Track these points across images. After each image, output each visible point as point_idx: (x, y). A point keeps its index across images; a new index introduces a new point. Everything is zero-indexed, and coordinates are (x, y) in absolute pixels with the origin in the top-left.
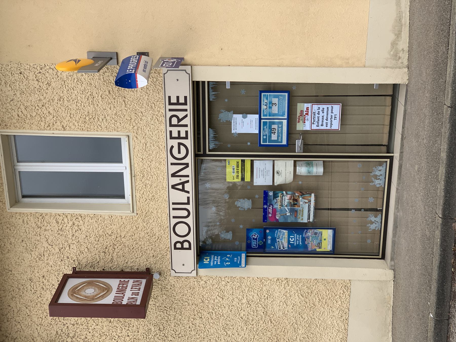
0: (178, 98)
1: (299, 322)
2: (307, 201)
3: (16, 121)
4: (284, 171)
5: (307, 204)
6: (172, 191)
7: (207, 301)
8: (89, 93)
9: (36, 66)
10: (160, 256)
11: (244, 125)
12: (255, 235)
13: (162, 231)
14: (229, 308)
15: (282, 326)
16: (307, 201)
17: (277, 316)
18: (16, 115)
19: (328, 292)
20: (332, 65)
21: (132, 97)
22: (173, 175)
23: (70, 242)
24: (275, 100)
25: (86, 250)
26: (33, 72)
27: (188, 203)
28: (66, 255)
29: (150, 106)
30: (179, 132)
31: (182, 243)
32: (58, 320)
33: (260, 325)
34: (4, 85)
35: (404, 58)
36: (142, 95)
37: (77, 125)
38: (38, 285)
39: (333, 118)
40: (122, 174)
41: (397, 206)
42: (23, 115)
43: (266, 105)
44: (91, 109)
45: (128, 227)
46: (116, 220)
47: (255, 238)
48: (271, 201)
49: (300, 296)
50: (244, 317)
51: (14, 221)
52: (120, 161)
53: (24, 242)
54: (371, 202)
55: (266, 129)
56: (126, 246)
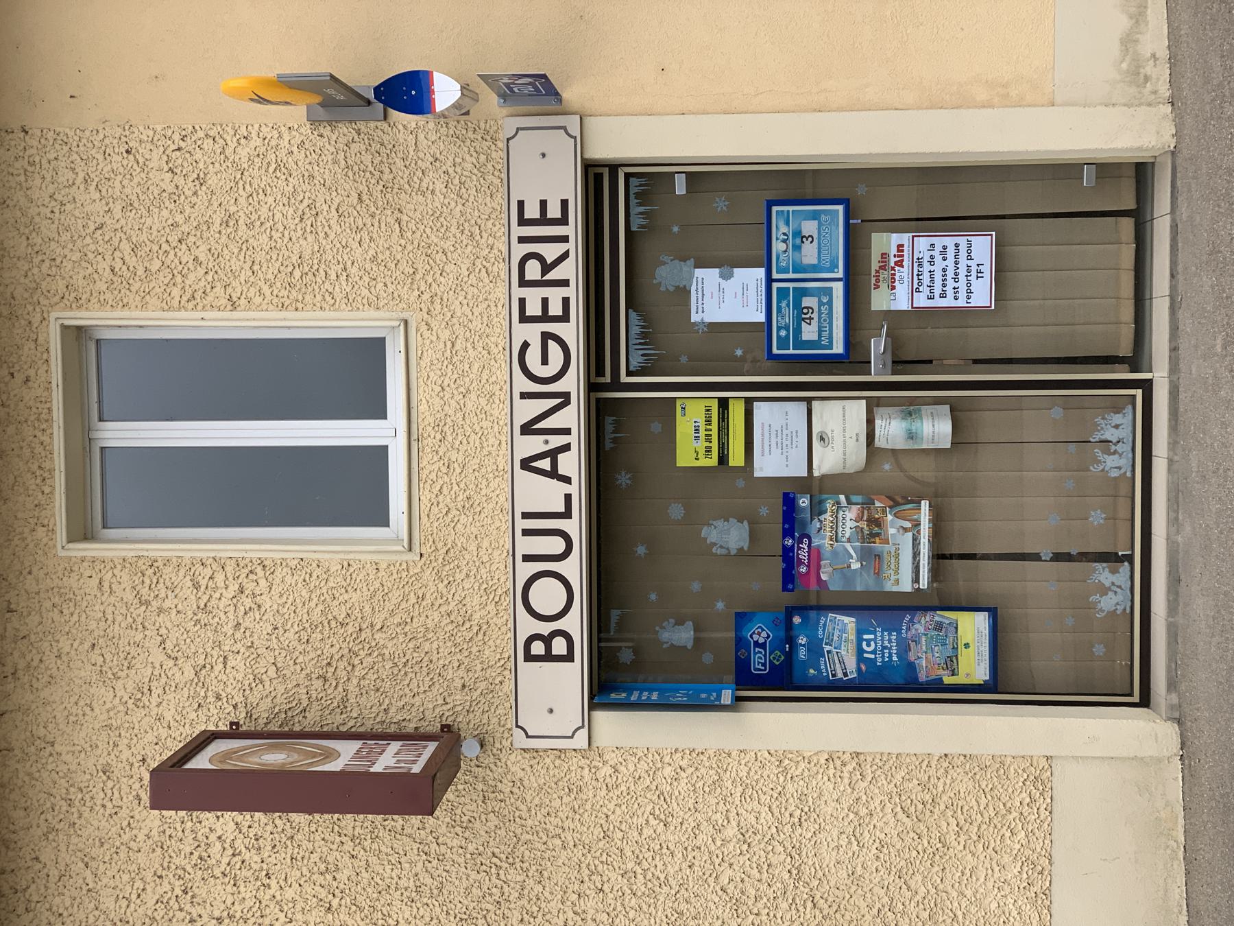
0: (543, 204)
1: (899, 905)
2: (908, 525)
3: (104, 287)
4: (839, 431)
5: (910, 534)
6: (522, 476)
7: (620, 835)
8: (306, 202)
9: (169, 133)
10: (483, 685)
11: (727, 297)
12: (759, 632)
13: (491, 607)
14: (685, 858)
15: (847, 917)
16: (908, 525)
17: (832, 884)
18: (108, 270)
19: (983, 801)
20: (963, 102)
21: (421, 208)
22: (527, 429)
23: (227, 648)
24: (809, 227)
25: (272, 672)
26: (162, 149)
27: (567, 514)
28: (214, 687)
29: (466, 232)
30: (545, 301)
31: (547, 640)
32: (176, 906)
33: (779, 916)
34: (82, 187)
35: (1158, 79)
36: (446, 201)
37: (268, 293)
38: (125, 789)
39: (974, 273)
40: (384, 449)
41: (1173, 515)
42: (124, 268)
43: (784, 241)
44: (308, 246)
45: (395, 597)
46: (361, 576)
47: (761, 641)
48: (804, 524)
49: (901, 815)
50: (732, 886)
51: (75, 586)
52: (381, 414)
53: (97, 651)
54: (1096, 528)
55: (785, 310)
56: (387, 656)
